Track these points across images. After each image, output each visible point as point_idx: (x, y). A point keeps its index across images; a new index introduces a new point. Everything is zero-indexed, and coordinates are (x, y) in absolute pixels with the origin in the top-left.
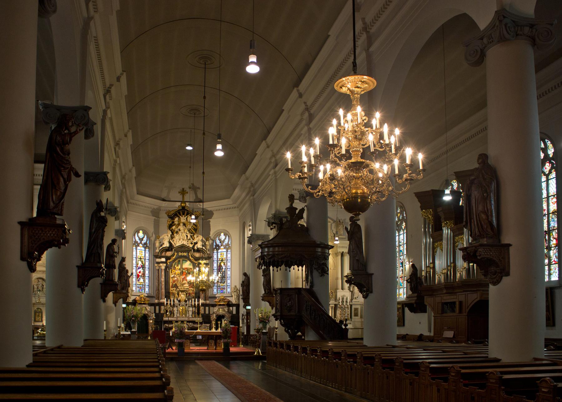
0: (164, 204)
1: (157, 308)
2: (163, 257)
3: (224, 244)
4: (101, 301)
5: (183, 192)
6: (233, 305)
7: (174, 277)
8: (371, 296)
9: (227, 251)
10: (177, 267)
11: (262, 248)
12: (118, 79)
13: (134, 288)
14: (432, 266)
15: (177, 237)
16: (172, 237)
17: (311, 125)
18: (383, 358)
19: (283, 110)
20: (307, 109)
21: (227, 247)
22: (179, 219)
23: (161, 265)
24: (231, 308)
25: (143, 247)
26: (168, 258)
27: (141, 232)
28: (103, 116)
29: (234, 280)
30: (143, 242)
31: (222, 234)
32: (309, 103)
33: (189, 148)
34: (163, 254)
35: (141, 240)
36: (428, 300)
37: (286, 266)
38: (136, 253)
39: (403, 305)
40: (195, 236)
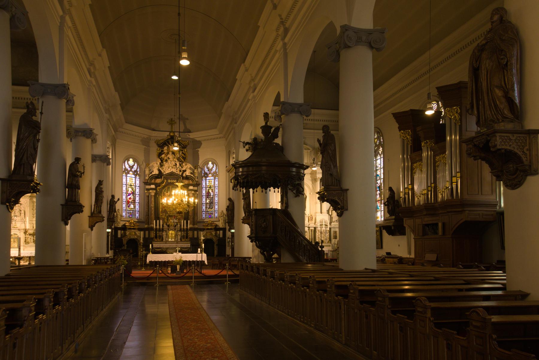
1: (147, 232)
2: (153, 184)
4: (62, 224)
5: (171, 122)
6: (220, 229)
11: (236, 168)
13: (124, 214)
15: (166, 165)
16: (161, 165)
17: (286, 40)
19: (259, 26)
20: (282, 23)
21: (215, 175)
22: (168, 148)
23: (151, 191)
24: (218, 232)
25: (133, 174)
26: (157, 185)
27: (131, 160)
28: (60, 23)
29: (220, 206)
30: (133, 170)
31: (210, 163)
32: (284, 16)
33: (175, 78)
34: (153, 181)
35: (132, 167)
36: (407, 223)
37: (262, 188)
38: (126, 180)
39: (382, 228)
40: (184, 164)
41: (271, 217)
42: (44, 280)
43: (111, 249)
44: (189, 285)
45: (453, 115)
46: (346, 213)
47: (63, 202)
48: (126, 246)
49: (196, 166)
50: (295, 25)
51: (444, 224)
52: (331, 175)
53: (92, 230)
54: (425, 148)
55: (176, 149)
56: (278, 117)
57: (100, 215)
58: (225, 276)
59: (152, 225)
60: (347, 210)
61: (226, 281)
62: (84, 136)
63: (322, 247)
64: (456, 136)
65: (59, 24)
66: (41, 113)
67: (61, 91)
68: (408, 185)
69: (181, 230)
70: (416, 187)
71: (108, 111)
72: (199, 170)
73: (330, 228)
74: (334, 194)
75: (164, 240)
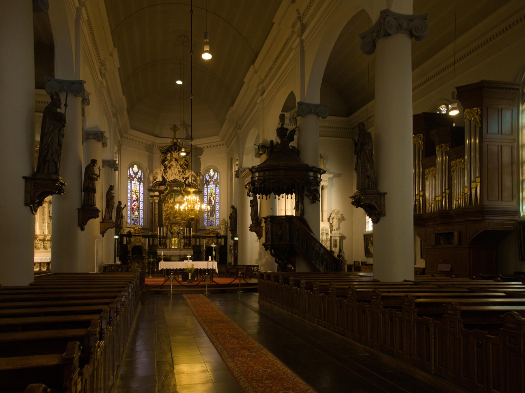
0: (158, 140)
2: (157, 191)
3: (213, 180)
4: (79, 229)
5: (175, 129)
6: (221, 237)
7: (167, 210)
9: (216, 187)
13: (129, 221)
14: (421, 193)
15: (169, 172)
16: (165, 172)
17: (304, 37)
19: (274, 23)
20: (300, 18)
21: (216, 183)
22: (172, 155)
23: (155, 198)
24: (220, 240)
25: (138, 181)
26: (161, 192)
27: (135, 166)
30: (137, 176)
31: (212, 170)
32: (302, 11)
33: (179, 82)
34: (157, 188)
35: (136, 174)
38: (131, 187)
40: (187, 171)
41: (288, 224)
42: (57, 289)
43: (117, 256)
44: (203, 293)
45: (473, 116)
46: (382, 219)
47: (79, 207)
48: (131, 252)
49: (198, 174)
50: (313, 23)
51: (460, 234)
52: (368, 177)
53: (103, 236)
54: (440, 152)
55: (183, 154)
56: (294, 119)
57: (111, 221)
58: (237, 285)
59: (156, 233)
60: (384, 215)
61: (238, 290)
62: (95, 139)
64: (475, 139)
65: (75, 17)
66: (66, 105)
67: (77, 88)
68: (419, 191)
69: (184, 238)
70: (427, 194)
71: (115, 115)
72: (201, 177)
73: (331, 237)
74: (369, 198)
75: (168, 248)
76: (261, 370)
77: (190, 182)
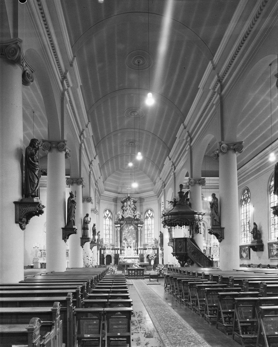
1: (116, 251)
2: (119, 224)
7: (125, 234)
8: (224, 241)
10: (126, 229)
12: (87, 127)
16: (123, 213)
17: (192, 144)
18: (223, 277)
19: (177, 138)
21: (152, 217)
23: (118, 228)
25: (109, 219)
30: (109, 216)
32: (174, 162)
35: (108, 215)
38: (105, 222)
40: (135, 212)
47: (81, 237)
63: (212, 259)
66: (75, 196)
76: (186, 343)
77: (137, 218)
